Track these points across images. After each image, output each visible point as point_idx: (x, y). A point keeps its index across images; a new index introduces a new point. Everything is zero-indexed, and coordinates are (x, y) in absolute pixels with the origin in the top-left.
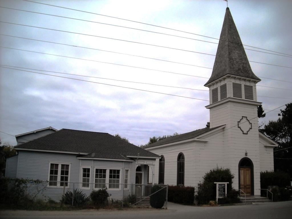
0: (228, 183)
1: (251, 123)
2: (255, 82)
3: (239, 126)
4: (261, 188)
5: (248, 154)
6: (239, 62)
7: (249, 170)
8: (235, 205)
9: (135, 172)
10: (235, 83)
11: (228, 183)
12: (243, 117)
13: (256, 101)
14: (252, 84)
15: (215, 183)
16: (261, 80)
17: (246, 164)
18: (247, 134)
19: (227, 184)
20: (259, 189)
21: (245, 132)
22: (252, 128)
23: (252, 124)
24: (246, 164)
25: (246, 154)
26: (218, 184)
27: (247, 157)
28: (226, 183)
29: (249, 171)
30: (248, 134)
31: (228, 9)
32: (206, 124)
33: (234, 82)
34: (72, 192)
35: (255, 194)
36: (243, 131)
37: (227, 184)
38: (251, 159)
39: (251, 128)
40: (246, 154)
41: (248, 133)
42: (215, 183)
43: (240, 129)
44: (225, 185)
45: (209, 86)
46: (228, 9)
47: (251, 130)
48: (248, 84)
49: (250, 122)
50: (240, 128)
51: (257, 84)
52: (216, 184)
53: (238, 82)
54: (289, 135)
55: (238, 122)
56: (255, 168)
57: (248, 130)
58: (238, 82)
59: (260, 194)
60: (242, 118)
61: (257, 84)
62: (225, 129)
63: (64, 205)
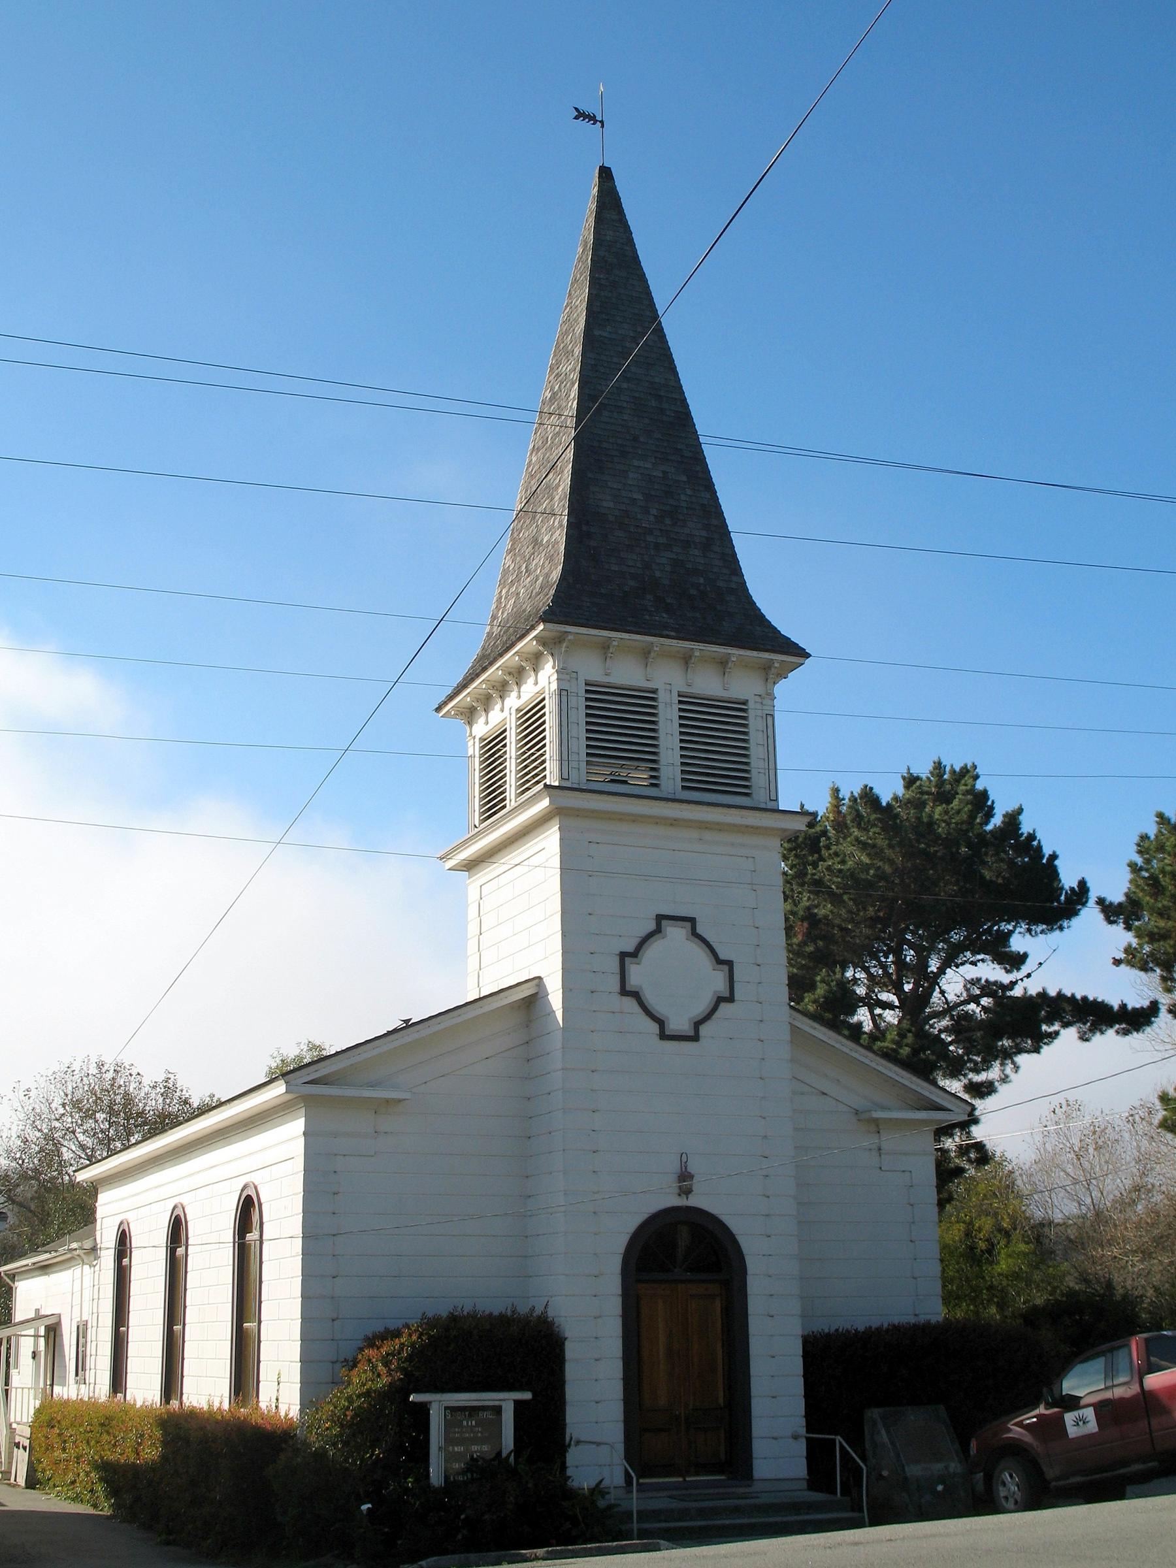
0: (527, 1396)
1: (729, 964)
2: (771, 675)
3: (726, 968)
4: (810, 1428)
5: (697, 1186)
6: (650, 538)
8: (525, 1559)
9: (676, 1185)
10: (605, 680)
11: (527, 1396)
12: (660, 918)
13: (770, 805)
14: (741, 685)
16: (808, 656)
17: (684, 1259)
19: (518, 1404)
20: (795, 1437)
23: (615, 985)
24: (684, 1259)
27: (693, 1201)
28: (507, 1400)
31: (605, 174)
32: (1136, 839)
33: (597, 675)
36: (661, 1023)
37: (518, 1404)
38: (726, 1219)
39: (727, 994)
40: (685, 1177)
41: (704, 1030)
43: (637, 1008)
44: (498, 1410)
46: (605, 174)
48: (707, 683)
49: (723, 956)
50: (636, 995)
51: (782, 689)
52: (424, 1408)
53: (626, 673)
54: (1006, 1043)
55: (623, 956)
56: (757, 1286)
57: (701, 1006)
59: (799, 1468)
60: (652, 926)
61: (783, 682)
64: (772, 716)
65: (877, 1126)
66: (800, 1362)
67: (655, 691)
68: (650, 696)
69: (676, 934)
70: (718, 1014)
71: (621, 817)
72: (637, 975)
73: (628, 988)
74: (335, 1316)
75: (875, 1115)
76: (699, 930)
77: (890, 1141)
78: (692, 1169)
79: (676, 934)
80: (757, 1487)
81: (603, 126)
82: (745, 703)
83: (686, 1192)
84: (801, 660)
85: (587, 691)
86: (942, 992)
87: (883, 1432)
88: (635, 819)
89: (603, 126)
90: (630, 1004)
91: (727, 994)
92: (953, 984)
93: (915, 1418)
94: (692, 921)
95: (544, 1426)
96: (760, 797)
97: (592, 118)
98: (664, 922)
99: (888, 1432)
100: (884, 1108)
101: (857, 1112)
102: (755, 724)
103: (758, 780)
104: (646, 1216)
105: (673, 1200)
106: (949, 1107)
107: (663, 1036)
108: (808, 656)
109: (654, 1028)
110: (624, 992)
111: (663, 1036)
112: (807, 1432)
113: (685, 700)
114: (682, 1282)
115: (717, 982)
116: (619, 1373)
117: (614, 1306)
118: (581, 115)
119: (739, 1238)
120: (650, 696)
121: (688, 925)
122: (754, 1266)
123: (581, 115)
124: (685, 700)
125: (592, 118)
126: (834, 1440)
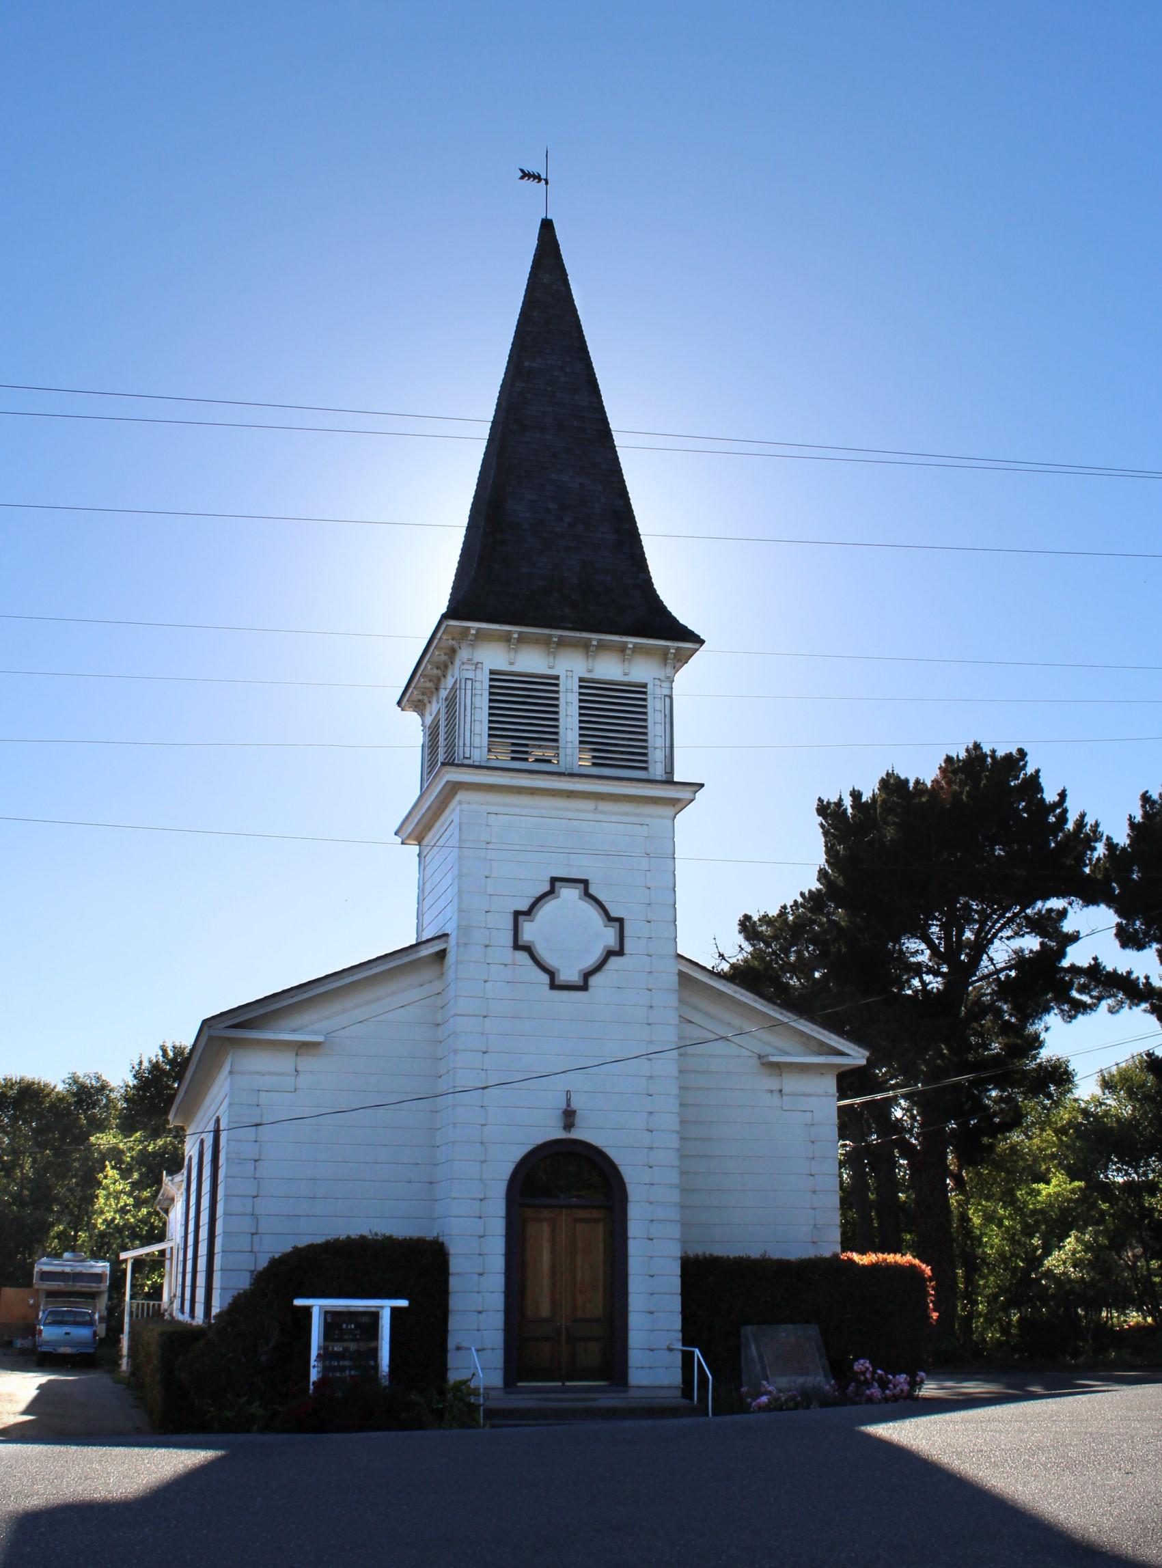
0: (403, 1303)
7: (597, 1221)
11: (403, 1303)
12: (554, 880)
14: (642, 671)
15: (298, 1302)
17: (566, 1184)
18: (584, 987)
19: (394, 1310)
21: (569, 975)
22: (627, 949)
25: (569, 1117)
26: (318, 1306)
27: (575, 1134)
28: (385, 1307)
29: (601, 1226)
30: (591, 990)
34: (1045, 1054)
35: (637, 1377)
37: (394, 1310)
40: (569, 1117)
41: (593, 981)
42: (298, 1302)
43: (530, 962)
45: (420, 707)
47: (614, 962)
48: (609, 669)
49: (613, 914)
50: (528, 949)
52: (307, 1310)
53: (531, 661)
55: (517, 914)
56: (635, 1212)
58: (531, 661)
60: (546, 887)
62: (451, 958)
63: (1077, 1093)
64: (671, 697)
65: (778, 1068)
66: (678, 1281)
67: (557, 678)
68: (552, 681)
69: (569, 895)
70: (607, 967)
71: (520, 790)
72: (529, 932)
73: (520, 943)
74: (254, 1231)
75: (773, 1059)
76: (592, 891)
77: (792, 1083)
78: (574, 1106)
79: (569, 895)
80: (633, 1393)
81: (547, 183)
82: (645, 686)
83: (569, 1126)
84: (696, 646)
85: (581, 687)
86: (991, 959)
87: (753, 1348)
88: (533, 791)
89: (547, 183)
90: (523, 957)
91: (617, 949)
92: (1001, 952)
93: (787, 1335)
94: (585, 883)
95: (425, 1331)
96: (658, 771)
97: (537, 178)
98: (558, 884)
99: (757, 1349)
100: (788, 1054)
101: (760, 1057)
102: (654, 706)
103: (657, 755)
104: (530, 1148)
105: (561, 1134)
106: (847, 1051)
107: (554, 986)
108: (702, 642)
109: (545, 978)
110: (517, 946)
111: (554, 986)
112: (684, 1345)
113: (585, 684)
114: (566, 1207)
115: (609, 937)
116: (678, 1307)
117: (497, 1227)
118: (526, 175)
119: (621, 1169)
120: (552, 681)
121: (582, 886)
122: (635, 1193)
123: (526, 175)
124: (585, 684)
125: (537, 178)
126: (693, 1353)
